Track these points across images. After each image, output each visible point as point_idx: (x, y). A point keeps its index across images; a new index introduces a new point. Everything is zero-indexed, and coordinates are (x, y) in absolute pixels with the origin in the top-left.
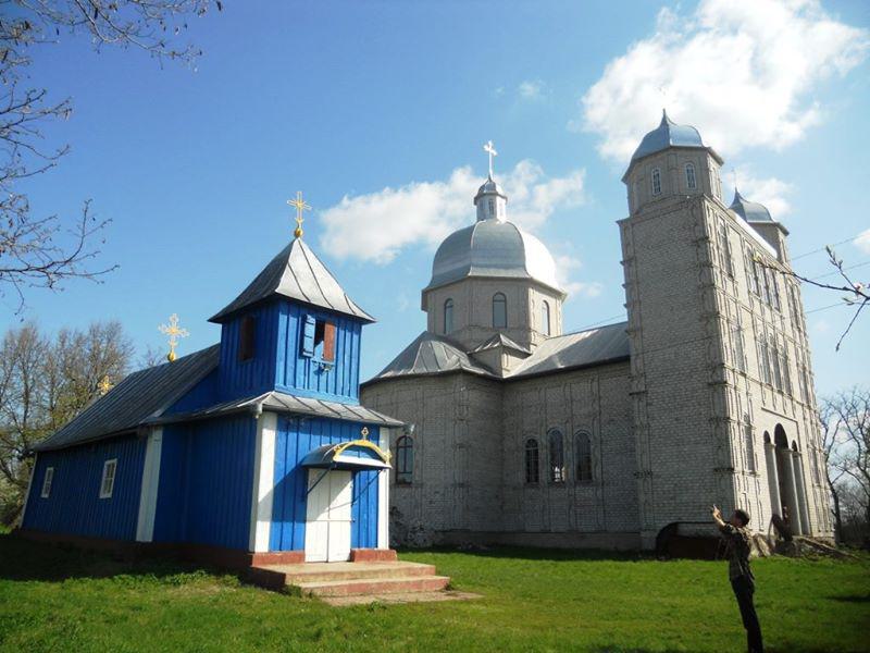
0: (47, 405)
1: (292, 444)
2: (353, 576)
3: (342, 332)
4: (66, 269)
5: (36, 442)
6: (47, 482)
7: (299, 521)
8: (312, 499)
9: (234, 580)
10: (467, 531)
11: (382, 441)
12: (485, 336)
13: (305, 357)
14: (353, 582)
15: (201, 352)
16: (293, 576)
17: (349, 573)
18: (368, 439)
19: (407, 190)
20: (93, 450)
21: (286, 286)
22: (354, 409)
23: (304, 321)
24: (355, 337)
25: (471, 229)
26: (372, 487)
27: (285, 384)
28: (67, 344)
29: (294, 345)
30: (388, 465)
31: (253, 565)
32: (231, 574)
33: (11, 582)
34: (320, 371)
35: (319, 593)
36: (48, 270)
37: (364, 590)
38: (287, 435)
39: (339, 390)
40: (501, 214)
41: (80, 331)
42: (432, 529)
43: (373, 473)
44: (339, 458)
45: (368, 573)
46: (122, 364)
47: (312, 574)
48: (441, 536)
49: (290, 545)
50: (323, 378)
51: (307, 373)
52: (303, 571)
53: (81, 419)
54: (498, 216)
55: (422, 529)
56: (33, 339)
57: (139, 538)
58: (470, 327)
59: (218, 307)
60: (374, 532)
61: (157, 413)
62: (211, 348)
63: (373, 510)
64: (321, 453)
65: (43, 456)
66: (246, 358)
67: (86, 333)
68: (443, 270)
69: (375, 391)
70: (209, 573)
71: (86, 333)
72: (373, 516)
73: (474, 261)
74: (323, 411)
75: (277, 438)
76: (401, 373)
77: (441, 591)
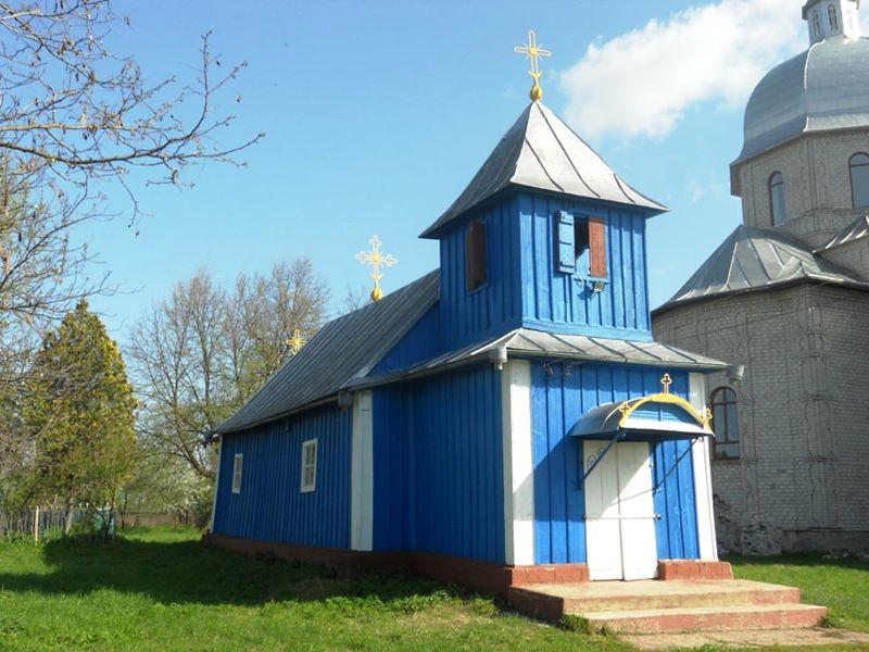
0: (231, 374)
1: (555, 407)
2: (666, 602)
3: (615, 232)
4: (190, 148)
5: (221, 422)
6: (237, 473)
7: (574, 520)
8: (591, 486)
9: (487, 605)
10: (838, 531)
11: (693, 394)
12: (840, 223)
13: (563, 274)
14: (668, 612)
15: (414, 284)
16: (574, 601)
17: (661, 598)
18: (672, 389)
19: (682, 20)
20: (287, 428)
21: (526, 172)
22: (645, 347)
23: (557, 220)
24: (637, 237)
25: (801, 59)
26: (685, 461)
27: (537, 317)
28: (247, 293)
29: (545, 266)
30: (707, 430)
31: (514, 585)
32: (484, 597)
33: (200, 606)
34: (587, 294)
35: (615, 628)
36: (162, 153)
37: (687, 625)
38: (547, 391)
39: (620, 319)
40: (851, 27)
41: (260, 275)
42: (779, 528)
43: (683, 444)
44: (627, 422)
45: (690, 597)
46: (316, 313)
47: (602, 600)
48: (793, 537)
49: (566, 555)
50: (593, 303)
51: (567, 298)
52: (589, 594)
53: (271, 388)
54: (846, 32)
55: (762, 527)
56: (206, 291)
57: (355, 546)
58: (813, 212)
59: (432, 216)
60: (691, 532)
61: (363, 373)
62: (428, 276)
63: (688, 501)
64: (600, 417)
65: (231, 439)
66: (477, 284)
67: (269, 277)
68: (759, 131)
69: (679, 319)
70: (453, 595)
71: (269, 277)
72: (687, 510)
73: (812, 108)
74: (597, 353)
75: (532, 398)
76: (709, 291)
77: (810, 628)
